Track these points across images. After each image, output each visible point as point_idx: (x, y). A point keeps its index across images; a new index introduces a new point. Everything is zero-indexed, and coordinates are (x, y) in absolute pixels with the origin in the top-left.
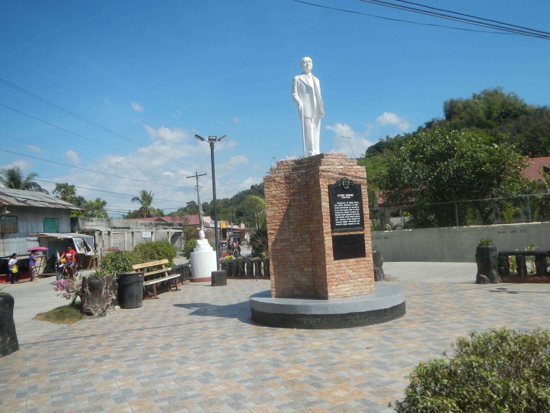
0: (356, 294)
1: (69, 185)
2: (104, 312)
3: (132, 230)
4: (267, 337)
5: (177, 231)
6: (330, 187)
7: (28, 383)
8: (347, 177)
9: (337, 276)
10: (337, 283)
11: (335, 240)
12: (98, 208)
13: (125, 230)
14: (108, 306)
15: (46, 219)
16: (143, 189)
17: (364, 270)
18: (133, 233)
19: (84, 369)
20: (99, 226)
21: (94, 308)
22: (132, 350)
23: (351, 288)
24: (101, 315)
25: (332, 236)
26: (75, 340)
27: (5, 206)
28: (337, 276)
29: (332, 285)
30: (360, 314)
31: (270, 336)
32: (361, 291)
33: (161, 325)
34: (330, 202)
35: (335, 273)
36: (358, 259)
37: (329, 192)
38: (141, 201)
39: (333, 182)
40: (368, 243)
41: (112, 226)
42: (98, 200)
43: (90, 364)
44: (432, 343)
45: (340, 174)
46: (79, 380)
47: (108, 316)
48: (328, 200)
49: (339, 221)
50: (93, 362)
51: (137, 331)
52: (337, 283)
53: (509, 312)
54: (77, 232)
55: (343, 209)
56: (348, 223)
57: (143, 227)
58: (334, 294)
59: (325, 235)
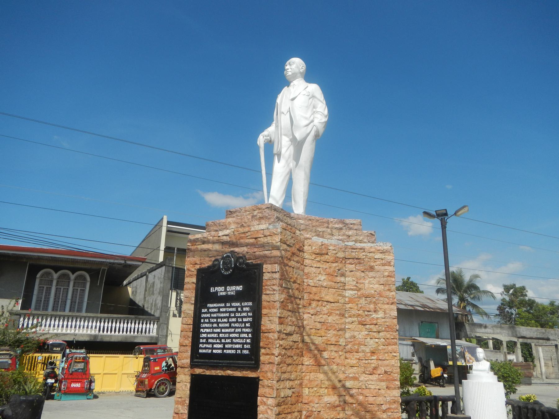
1: (517, 286)
3: (554, 343)
8: (236, 250)
13: (541, 341)
15: (422, 322)
20: (498, 333)
25: (192, 375)
34: (195, 304)
37: (197, 284)
39: (207, 263)
41: (519, 335)
45: (223, 243)
49: (207, 343)
54: (463, 339)
55: (217, 318)
56: (224, 348)
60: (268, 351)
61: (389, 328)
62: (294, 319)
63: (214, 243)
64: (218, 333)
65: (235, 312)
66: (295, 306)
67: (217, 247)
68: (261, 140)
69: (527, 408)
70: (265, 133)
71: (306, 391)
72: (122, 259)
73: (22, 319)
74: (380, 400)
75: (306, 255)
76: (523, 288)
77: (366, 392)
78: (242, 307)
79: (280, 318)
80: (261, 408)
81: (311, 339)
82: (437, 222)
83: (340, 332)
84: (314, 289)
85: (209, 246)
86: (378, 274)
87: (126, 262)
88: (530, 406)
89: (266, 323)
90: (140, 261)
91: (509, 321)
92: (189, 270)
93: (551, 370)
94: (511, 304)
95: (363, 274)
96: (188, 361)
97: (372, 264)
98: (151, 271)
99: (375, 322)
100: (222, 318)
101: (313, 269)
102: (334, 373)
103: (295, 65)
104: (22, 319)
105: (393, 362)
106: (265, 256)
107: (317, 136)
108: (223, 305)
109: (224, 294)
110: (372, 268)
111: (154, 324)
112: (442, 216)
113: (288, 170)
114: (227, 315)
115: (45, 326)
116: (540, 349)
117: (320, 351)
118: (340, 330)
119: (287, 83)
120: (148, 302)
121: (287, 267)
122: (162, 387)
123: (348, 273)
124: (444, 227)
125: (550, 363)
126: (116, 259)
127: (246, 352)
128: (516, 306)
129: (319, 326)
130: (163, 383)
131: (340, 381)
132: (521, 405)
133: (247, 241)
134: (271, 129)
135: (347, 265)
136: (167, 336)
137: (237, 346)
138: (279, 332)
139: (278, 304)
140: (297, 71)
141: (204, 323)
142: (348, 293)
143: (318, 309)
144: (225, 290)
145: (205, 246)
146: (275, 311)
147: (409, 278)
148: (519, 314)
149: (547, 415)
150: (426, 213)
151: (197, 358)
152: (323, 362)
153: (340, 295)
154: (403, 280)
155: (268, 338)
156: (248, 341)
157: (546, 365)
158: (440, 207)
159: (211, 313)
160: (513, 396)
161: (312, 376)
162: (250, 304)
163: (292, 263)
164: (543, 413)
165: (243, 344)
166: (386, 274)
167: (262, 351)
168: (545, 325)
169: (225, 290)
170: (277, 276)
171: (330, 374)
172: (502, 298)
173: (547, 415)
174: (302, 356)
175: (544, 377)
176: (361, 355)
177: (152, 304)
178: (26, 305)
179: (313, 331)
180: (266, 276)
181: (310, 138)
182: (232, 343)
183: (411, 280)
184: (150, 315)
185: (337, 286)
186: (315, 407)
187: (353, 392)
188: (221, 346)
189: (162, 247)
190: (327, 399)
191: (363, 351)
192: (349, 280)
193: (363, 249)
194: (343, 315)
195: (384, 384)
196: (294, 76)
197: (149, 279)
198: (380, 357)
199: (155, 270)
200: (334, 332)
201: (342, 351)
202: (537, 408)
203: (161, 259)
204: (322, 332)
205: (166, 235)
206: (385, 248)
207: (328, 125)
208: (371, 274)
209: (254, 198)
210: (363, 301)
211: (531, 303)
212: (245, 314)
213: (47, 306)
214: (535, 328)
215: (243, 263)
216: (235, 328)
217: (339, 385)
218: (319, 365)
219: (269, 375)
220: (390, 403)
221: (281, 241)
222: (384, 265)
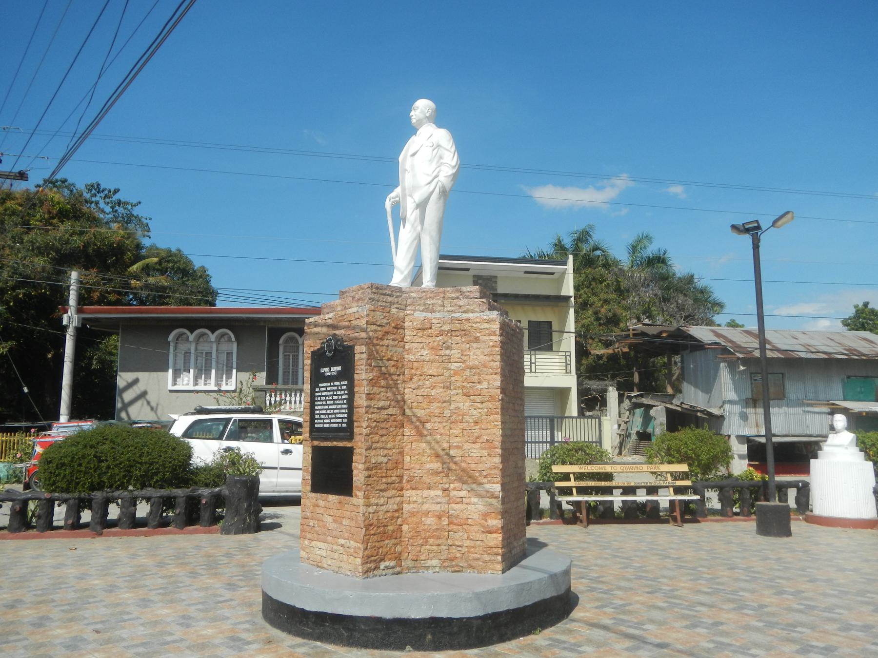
4: (247, 622)
8: (337, 332)
15: (849, 377)
27: (738, 358)
31: (240, 623)
34: (311, 384)
36: (342, 497)
40: (357, 468)
45: (328, 326)
61: (492, 398)
62: (389, 394)
66: (391, 382)
68: (388, 204)
70: (393, 195)
71: (407, 459)
73: (268, 397)
74: (481, 467)
77: (469, 460)
79: (368, 394)
81: (413, 412)
83: (445, 404)
84: (415, 364)
86: (483, 345)
95: (468, 346)
99: (479, 393)
101: (415, 345)
104: (268, 397)
106: (356, 338)
108: (328, 384)
110: (477, 339)
112: (753, 230)
113: (415, 235)
115: (295, 402)
117: (423, 423)
119: (413, 131)
121: (378, 347)
123: (454, 346)
124: (756, 247)
127: (344, 425)
129: (420, 399)
131: (443, 450)
134: (398, 191)
135: (453, 338)
138: (368, 407)
139: (365, 383)
140: (421, 116)
142: (454, 366)
143: (420, 383)
144: (330, 371)
147: (866, 305)
152: (425, 433)
153: (445, 368)
154: (856, 307)
155: (358, 412)
162: (346, 383)
163: (385, 342)
166: (491, 344)
167: (355, 424)
171: (433, 444)
174: (403, 427)
176: (465, 425)
178: (272, 378)
179: (415, 404)
180: (357, 357)
181: (434, 197)
183: (870, 306)
185: (441, 359)
186: (417, 473)
187: (457, 459)
191: (467, 422)
194: (448, 388)
195: (485, 452)
196: (420, 123)
198: (483, 427)
200: (439, 405)
201: (446, 422)
204: (424, 405)
206: (491, 317)
208: (475, 345)
209: (613, 186)
213: (297, 379)
217: (442, 453)
218: (421, 435)
220: (491, 469)
221: (367, 323)
222: (489, 335)
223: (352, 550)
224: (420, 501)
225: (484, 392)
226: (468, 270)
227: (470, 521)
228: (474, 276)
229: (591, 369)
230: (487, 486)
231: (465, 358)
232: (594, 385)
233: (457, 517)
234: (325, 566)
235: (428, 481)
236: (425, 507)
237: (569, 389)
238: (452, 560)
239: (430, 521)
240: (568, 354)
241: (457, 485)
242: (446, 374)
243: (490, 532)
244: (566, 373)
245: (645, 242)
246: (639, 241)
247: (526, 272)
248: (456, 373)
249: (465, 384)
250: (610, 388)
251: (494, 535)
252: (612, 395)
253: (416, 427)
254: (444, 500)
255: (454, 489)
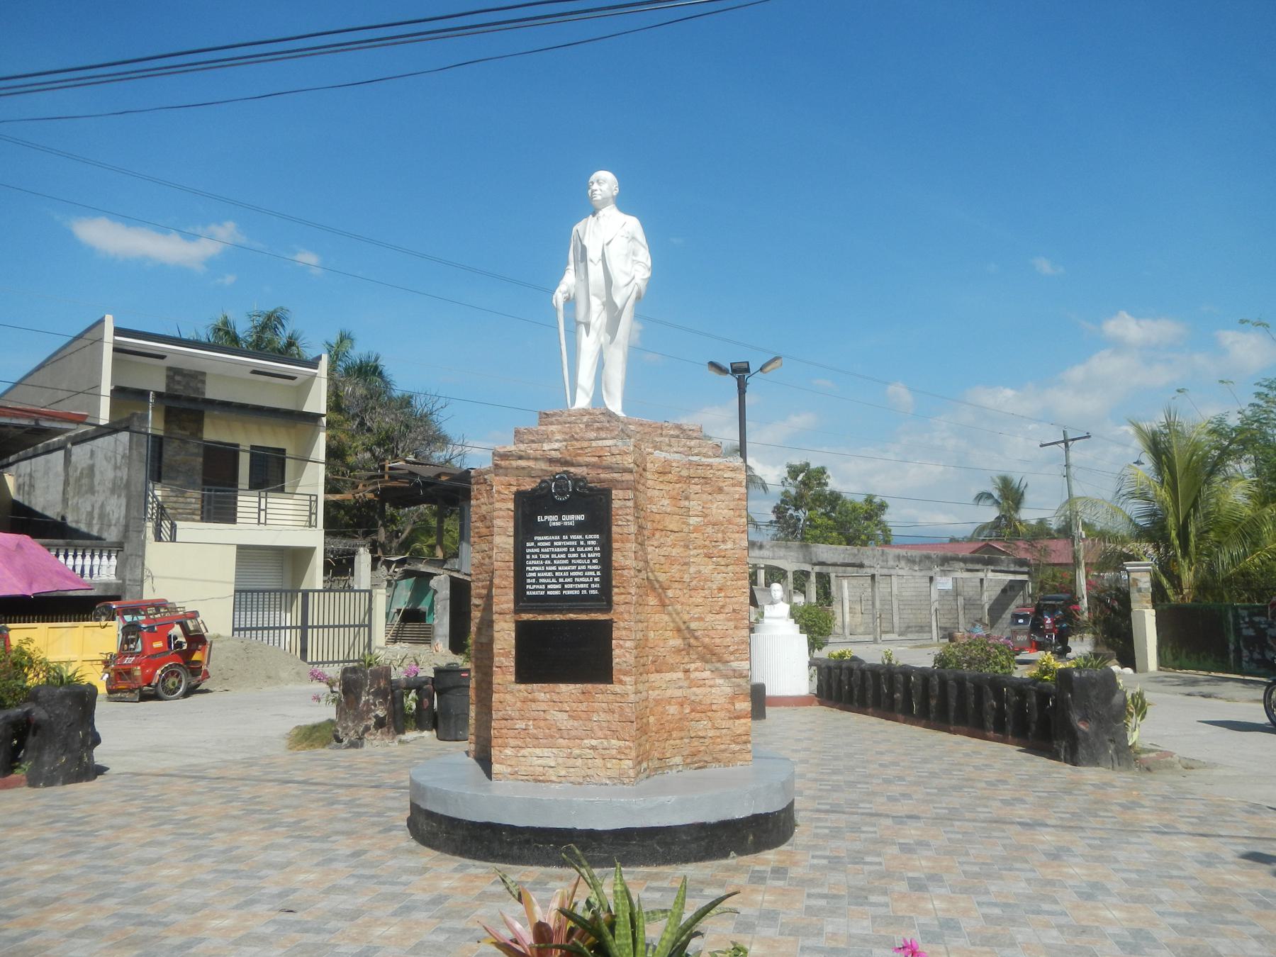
0: (572, 779)
2: (360, 739)
3: (870, 571)
5: (1019, 577)
6: (520, 497)
7: (763, 901)
8: (572, 470)
9: (521, 725)
10: (519, 743)
11: (523, 631)
12: (869, 517)
13: (849, 569)
14: (367, 729)
16: (1002, 474)
17: (603, 716)
18: (873, 577)
19: (882, 899)
20: (780, 558)
21: (345, 728)
22: (1001, 878)
23: (560, 760)
24: (353, 745)
26: (873, 819)
28: (521, 725)
29: (506, 746)
30: (512, 829)
32: (590, 772)
33: (1084, 824)
34: (516, 535)
35: (515, 714)
36: (589, 686)
38: (997, 502)
39: (528, 485)
41: (814, 560)
42: (869, 500)
43: (897, 888)
44: (116, 900)
45: (551, 461)
46: (867, 923)
47: (367, 746)
48: (511, 531)
50: (902, 887)
51: (1018, 828)
52: (519, 743)
53: (231, 867)
55: (550, 553)
56: (563, 589)
57: (903, 564)
58: (509, 770)
59: (495, 617)
60: (622, 590)
63: (536, 459)
64: (554, 572)
65: (575, 547)
67: (543, 465)
68: (559, 297)
69: (841, 669)
71: (652, 634)
72: (29, 417)
74: (728, 641)
75: (649, 475)
76: (822, 471)
77: (712, 633)
78: (586, 541)
80: (616, 652)
82: (731, 382)
85: (531, 464)
87: (37, 424)
88: (844, 666)
89: (617, 558)
90: (71, 421)
91: (793, 533)
92: (499, 492)
93: (859, 618)
94: (798, 502)
96: (511, 606)
97: (721, 484)
98: (80, 440)
100: (557, 553)
101: (657, 493)
102: (678, 614)
103: (604, 183)
105: (742, 599)
107: (638, 298)
109: (558, 524)
110: (720, 490)
111: (109, 557)
112: (740, 371)
114: (565, 549)
116: (845, 583)
117: (664, 589)
118: (685, 564)
120: (77, 508)
122: (172, 680)
123: (692, 496)
125: (858, 608)
126: (17, 417)
127: (595, 592)
128: (807, 504)
130: (173, 673)
132: (832, 664)
133: (587, 459)
136: (142, 581)
137: (582, 586)
140: (609, 194)
141: (531, 559)
142: (693, 521)
145: (522, 463)
146: (629, 545)
148: (810, 519)
149: (869, 674)
150: (713, 365)
151: (522, 600)
153: (684, 523)
156: (597, 579)
157: (852, 611)
158: (739, 358)
159: (540, 547)
160: (817, 654)
161: (657, 617)
162: (597, 536)
164: (863, 672)
165: (590, 583)
167: (615, 590)
168: (854, 538)
169: (560, 519)
170: (631, 504)
172: (783, 489)
173: (869, 674)
175: (847, 632)
177: (90, 514)
180: (616, 504)
182: (574, 582)
184: (88, 536)
186: (661, 651)
187: (698, 634)
188: (559, 586)
189: (106, 388)
190: (672, 643)
192: (695, 505)
193: (710, 466)
195: (732, 624)
196: (605, 203)
197: (74, 458)
199: (94, 438)
202: (855, 665)
203: (104, 417)
204: (666, 567)
205: (114, 360)
207: (651, 282)
208: (720, 497)
210: (709, 529)
211: (835, 499)
212: (590, 549)
214: (842, 547)
215: (584, 487)
216: (578, 565)
217: (683, 627)
218: (664, 605)
219: (626, 616)
220: (738, 644)
222: (733, 485)
223: (614, 752)
224: (664, 686)
225: (729, 553)
226: (162, 357)
227: (714, 707)
228: (169, 369)
229: (343, 521)
230: (735, 665)
231: (706, 511)
232: (340, 544)
233: (700, 703)
234: (554, 778)
235: (671, 661)
236: (669, 693)
237: (314, 548)
238: (694, 755)
239: (673, 709)
240: (313, 498)
241: (698, 664)
242: (686, 530)
243: (738, 718)
244: (310, 526)
245: (268, 335)
246: (264, 327)
247: (254, 372)
248: (696, 530)
249: (707, 543)
250: (362, 550)
251: (743, 721)
252: (363, 559)
253: (659, 595)
254: (685, 684)
255: (696, 670)
